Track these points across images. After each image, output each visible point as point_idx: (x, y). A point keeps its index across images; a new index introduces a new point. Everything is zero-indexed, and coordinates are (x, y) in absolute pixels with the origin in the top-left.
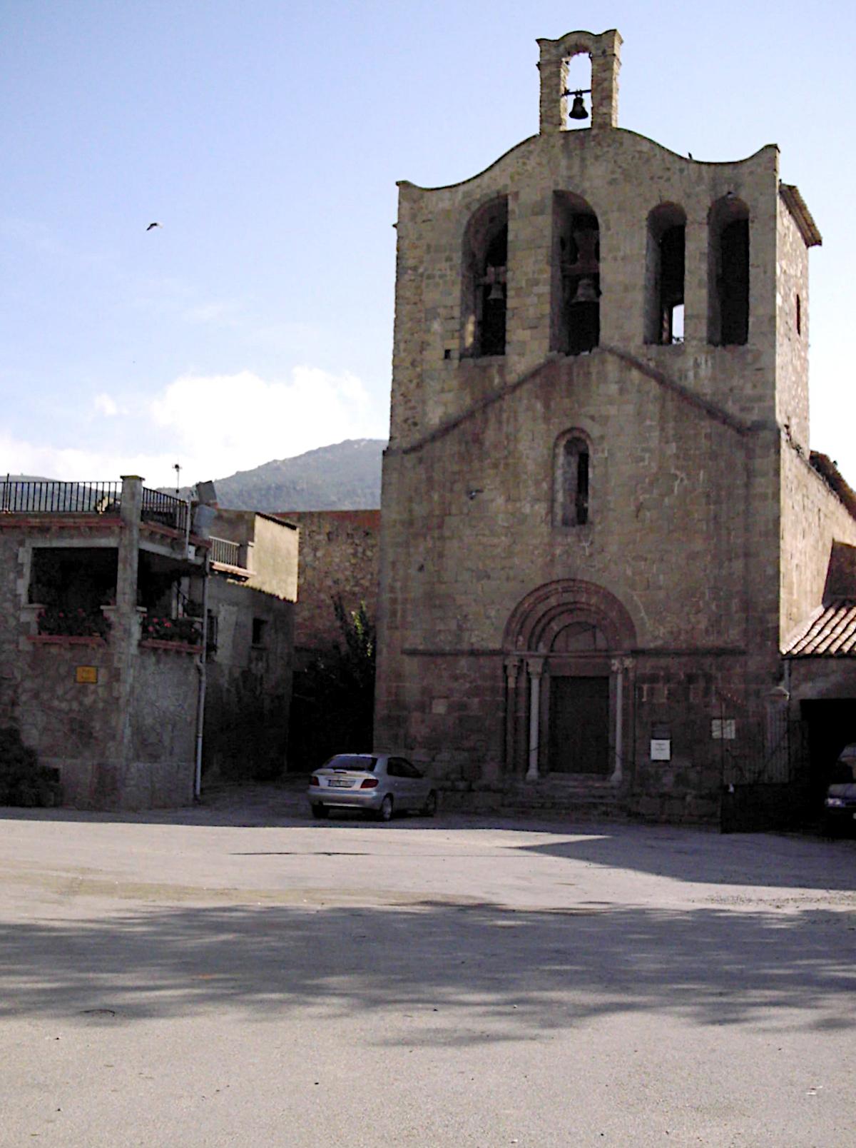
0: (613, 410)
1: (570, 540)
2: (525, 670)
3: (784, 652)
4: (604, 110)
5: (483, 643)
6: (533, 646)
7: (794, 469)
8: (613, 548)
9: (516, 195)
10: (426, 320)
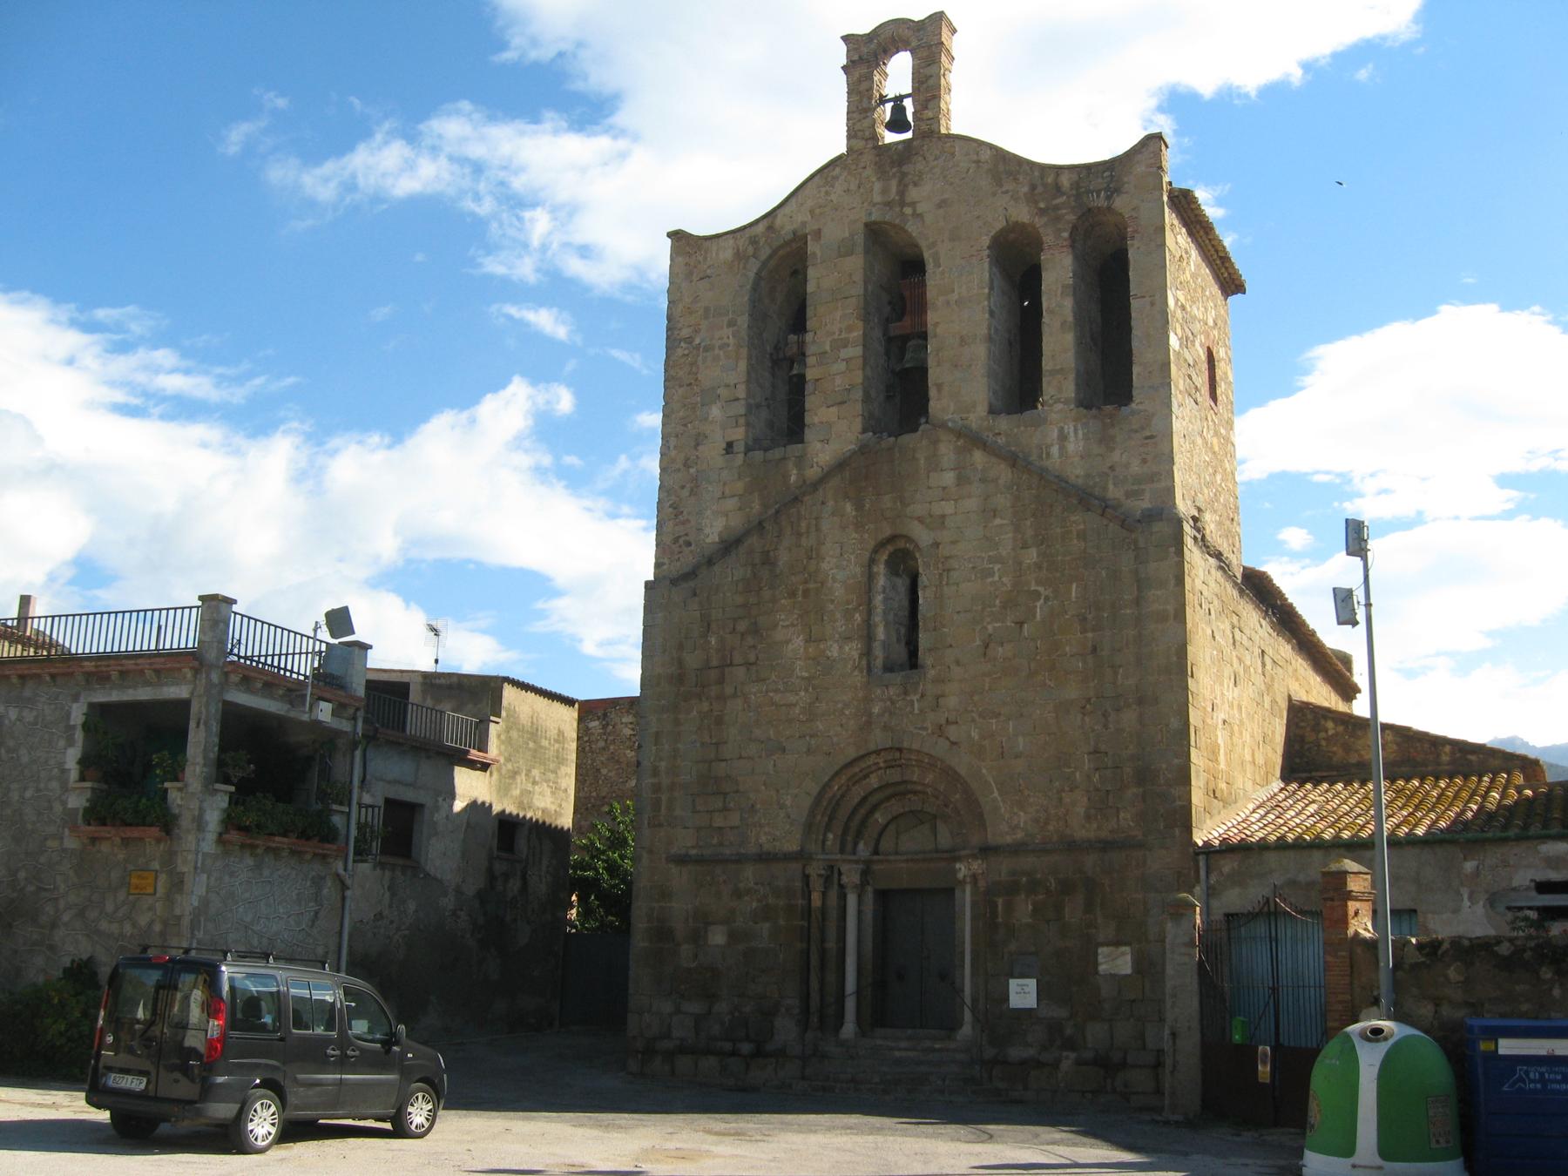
0: (948, 508)
1: (892, 691)
2: (836, 881)
3: (1200, 843)
4: (930, 114)
5: (777, 844)
6: (849, 847)
7: (1212, 584)
8: (952, 701)
9: (818, 233)
10: (702, 405)
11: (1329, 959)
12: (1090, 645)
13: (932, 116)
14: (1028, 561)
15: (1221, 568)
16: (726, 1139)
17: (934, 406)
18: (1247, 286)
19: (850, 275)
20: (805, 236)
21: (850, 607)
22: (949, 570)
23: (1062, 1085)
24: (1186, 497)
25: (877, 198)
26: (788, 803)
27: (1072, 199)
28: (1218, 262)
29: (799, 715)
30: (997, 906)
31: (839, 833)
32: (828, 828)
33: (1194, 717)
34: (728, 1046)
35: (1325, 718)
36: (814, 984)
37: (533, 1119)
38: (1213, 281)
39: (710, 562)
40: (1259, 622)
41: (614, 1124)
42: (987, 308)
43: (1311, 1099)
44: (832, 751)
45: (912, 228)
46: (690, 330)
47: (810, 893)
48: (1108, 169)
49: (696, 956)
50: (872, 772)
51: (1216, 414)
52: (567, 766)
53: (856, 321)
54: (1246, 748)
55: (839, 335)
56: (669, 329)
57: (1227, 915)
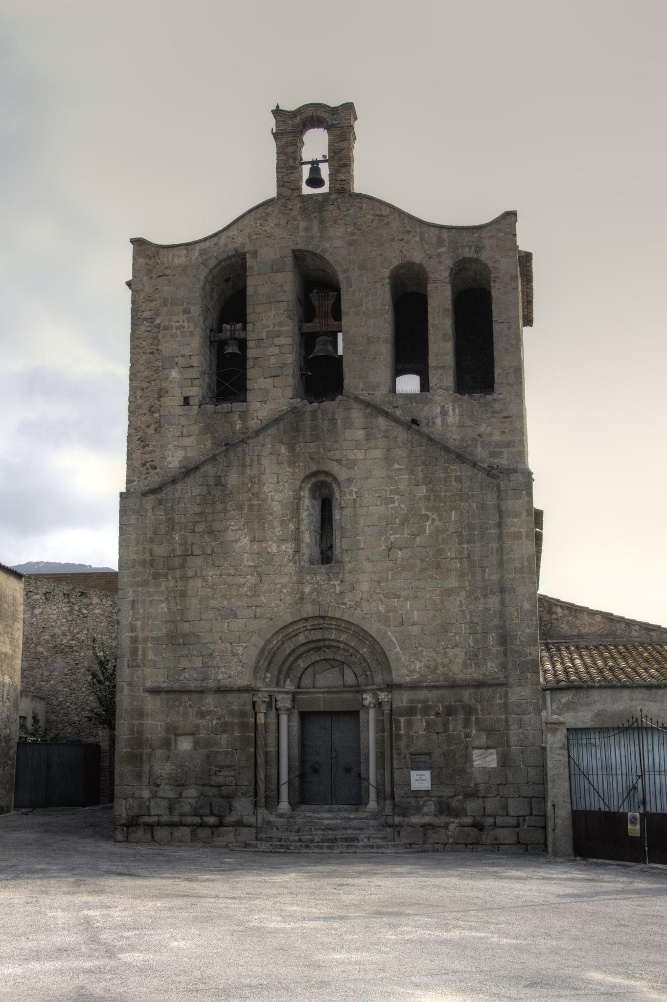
2: (274, 706)
6: (282, 682)
8: (365, 586)
13: (344, 179)
14: (420, 495)
21: (285, 518)
26: (240, 652)
29: (247, 591)
30: (400, 723)
31: (276, 673)
35: (556, 605)
39: (174, 482)
46: (151, 313)
53: (286, 319)
56: (133, 310)
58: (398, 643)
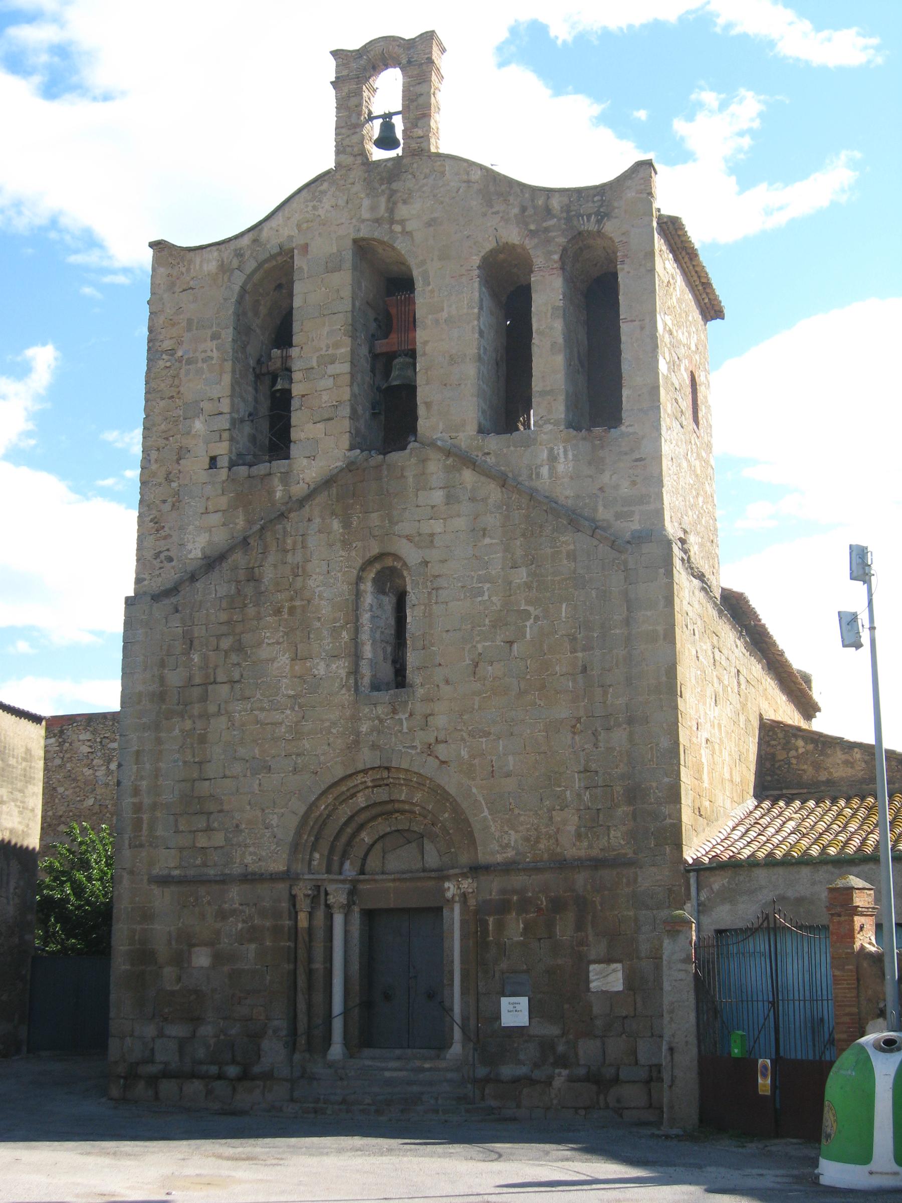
0: (437, 527)
1: (380, 710)
3: (690, 861)
4: (420, 133)
6: (335, 867)
7: (696, 605)
8: (440, 721)
11: (837, 973)
12: (580, 663)
13: (422, 135)
15: (703, 589)
16: (241, 1163)
17: (423, 424)
18: (725, 311)
19: (338, 291)
20: (292, 250)
21: (338, 624)
22: (437, 589)
23: (555, 1102)
24: (674, 519)
25: (366, 214)
26: (274, 822)
27: (563, 221)
28: (700, 288)
29: (285, 733)
30: (488, 924)
31: (326, 853)
32: (314, 848)
33: (683, 739)
34: (214, 1069)
35: (795, 736)
36: (302, 1006)
37: (34, 1148)
38: (695, 307)
39: (193, 578)
40: (735, 642)
41: (121, 1152)
42: (477, 328)
43: (826, 1109)
44: (319, 770)
45: (401, 245)
47: (296, 913)
48: (598, 194)
49: (179, 979)
50: (358, 792)
51: (698, 437)
52: (34, 784)
53: (344, 337)
54: (725, 766)
55: (327, 351)
56: (150, 341)
57: (719, 932)
58: (486, 804)
